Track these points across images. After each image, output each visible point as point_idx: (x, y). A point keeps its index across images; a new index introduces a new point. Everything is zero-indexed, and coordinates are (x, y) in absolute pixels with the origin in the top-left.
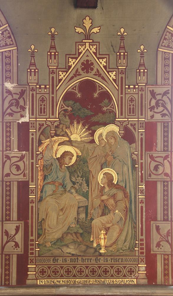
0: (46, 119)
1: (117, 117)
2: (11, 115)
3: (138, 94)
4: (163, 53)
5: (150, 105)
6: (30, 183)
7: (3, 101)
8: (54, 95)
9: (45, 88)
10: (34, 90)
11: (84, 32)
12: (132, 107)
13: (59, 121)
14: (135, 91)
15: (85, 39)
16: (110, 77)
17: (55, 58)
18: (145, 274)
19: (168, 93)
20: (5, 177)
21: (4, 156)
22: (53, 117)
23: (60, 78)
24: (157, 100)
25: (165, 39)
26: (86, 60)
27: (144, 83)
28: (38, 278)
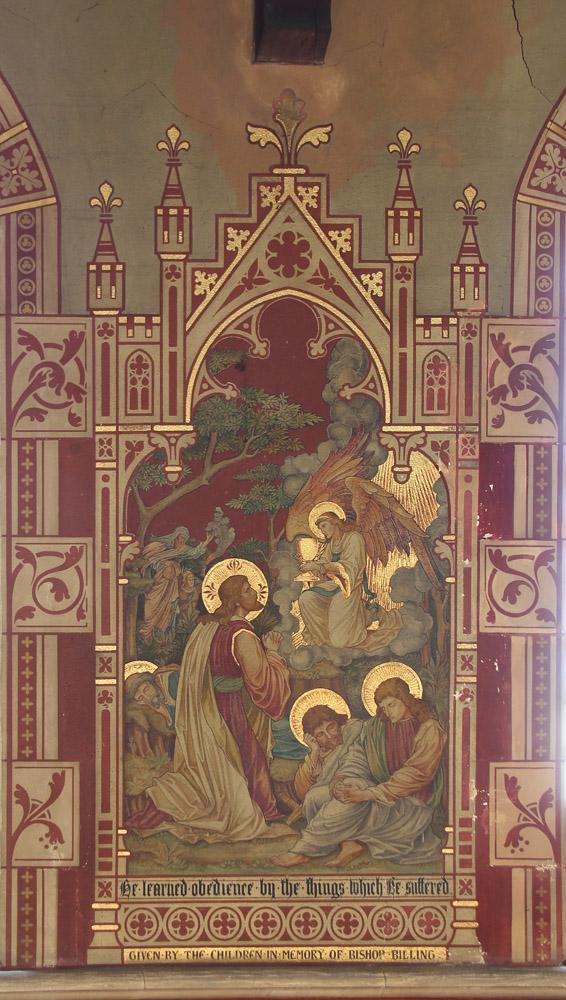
0: (152, 428)
1: (388, 421)
2: (36, 414)
4: (534, 209)
6: (100, 638)
8: (179, 349)
9: (149, 324)
10: (110, 333)
11: (277, 143)
12: (139, 387)
13: (194, 434)
14: (130, 334)
15: (282, 166)
16: (362, 290)
17: (180, 227)
18: (474, 931)
19: (552, 345)
20: (16, 620)
21: (14, 552)
23: (196, 293)
24: (513, 367)
25: (540, 164)
26: (284, 235)
27: (114, 309)
28: (125, 944)
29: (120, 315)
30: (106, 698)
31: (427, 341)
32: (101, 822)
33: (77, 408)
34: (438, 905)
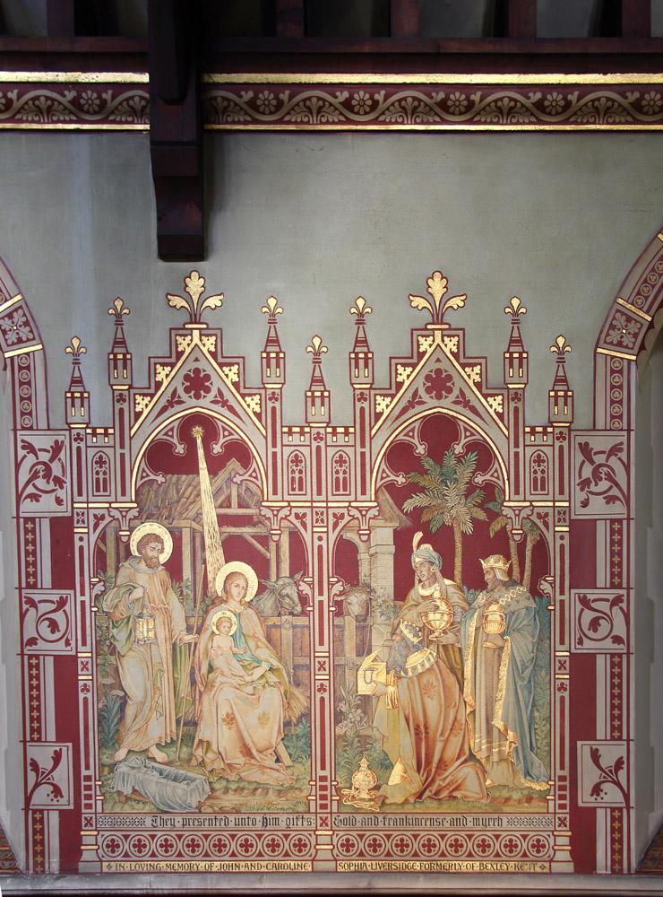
1: (507, 499)
2: (34, 497)
3: (553, 446)
5: (580, 477)
7: (18, 466)
8: (126, 451)
9: (106, 434)
10: (82, 440)
11: (187, 306)
13: (138, 509)
14: (95, 441)
15: (191, 323)
22: (274, 498)
27: (83, 424)
28: (103, 859)
29: (85, 428)
30: (86, 689)
31: (334, 444)
32: (85, 776)
33: (61, 494)
34: (545, 834)
